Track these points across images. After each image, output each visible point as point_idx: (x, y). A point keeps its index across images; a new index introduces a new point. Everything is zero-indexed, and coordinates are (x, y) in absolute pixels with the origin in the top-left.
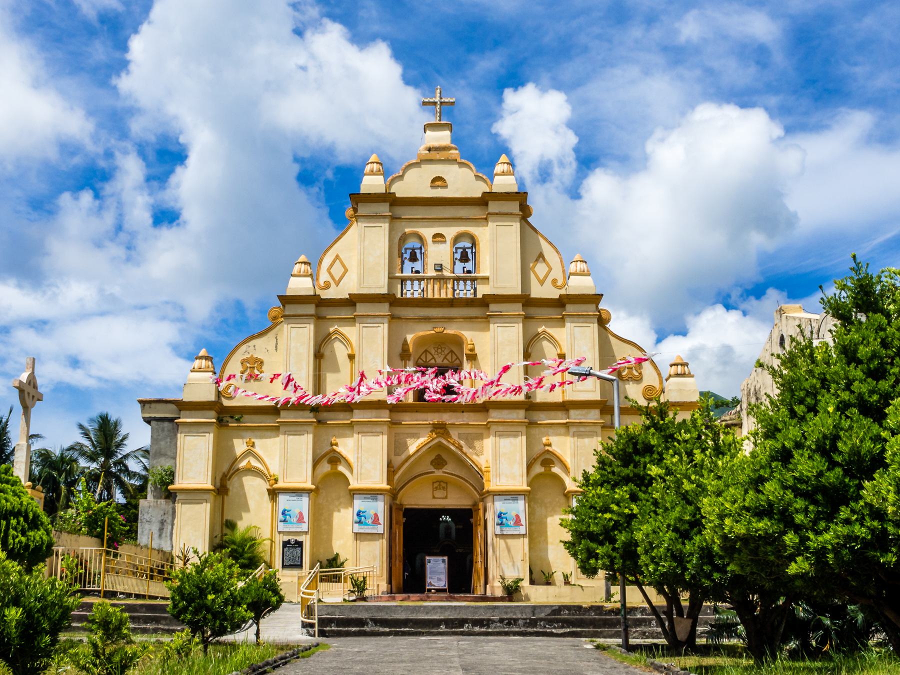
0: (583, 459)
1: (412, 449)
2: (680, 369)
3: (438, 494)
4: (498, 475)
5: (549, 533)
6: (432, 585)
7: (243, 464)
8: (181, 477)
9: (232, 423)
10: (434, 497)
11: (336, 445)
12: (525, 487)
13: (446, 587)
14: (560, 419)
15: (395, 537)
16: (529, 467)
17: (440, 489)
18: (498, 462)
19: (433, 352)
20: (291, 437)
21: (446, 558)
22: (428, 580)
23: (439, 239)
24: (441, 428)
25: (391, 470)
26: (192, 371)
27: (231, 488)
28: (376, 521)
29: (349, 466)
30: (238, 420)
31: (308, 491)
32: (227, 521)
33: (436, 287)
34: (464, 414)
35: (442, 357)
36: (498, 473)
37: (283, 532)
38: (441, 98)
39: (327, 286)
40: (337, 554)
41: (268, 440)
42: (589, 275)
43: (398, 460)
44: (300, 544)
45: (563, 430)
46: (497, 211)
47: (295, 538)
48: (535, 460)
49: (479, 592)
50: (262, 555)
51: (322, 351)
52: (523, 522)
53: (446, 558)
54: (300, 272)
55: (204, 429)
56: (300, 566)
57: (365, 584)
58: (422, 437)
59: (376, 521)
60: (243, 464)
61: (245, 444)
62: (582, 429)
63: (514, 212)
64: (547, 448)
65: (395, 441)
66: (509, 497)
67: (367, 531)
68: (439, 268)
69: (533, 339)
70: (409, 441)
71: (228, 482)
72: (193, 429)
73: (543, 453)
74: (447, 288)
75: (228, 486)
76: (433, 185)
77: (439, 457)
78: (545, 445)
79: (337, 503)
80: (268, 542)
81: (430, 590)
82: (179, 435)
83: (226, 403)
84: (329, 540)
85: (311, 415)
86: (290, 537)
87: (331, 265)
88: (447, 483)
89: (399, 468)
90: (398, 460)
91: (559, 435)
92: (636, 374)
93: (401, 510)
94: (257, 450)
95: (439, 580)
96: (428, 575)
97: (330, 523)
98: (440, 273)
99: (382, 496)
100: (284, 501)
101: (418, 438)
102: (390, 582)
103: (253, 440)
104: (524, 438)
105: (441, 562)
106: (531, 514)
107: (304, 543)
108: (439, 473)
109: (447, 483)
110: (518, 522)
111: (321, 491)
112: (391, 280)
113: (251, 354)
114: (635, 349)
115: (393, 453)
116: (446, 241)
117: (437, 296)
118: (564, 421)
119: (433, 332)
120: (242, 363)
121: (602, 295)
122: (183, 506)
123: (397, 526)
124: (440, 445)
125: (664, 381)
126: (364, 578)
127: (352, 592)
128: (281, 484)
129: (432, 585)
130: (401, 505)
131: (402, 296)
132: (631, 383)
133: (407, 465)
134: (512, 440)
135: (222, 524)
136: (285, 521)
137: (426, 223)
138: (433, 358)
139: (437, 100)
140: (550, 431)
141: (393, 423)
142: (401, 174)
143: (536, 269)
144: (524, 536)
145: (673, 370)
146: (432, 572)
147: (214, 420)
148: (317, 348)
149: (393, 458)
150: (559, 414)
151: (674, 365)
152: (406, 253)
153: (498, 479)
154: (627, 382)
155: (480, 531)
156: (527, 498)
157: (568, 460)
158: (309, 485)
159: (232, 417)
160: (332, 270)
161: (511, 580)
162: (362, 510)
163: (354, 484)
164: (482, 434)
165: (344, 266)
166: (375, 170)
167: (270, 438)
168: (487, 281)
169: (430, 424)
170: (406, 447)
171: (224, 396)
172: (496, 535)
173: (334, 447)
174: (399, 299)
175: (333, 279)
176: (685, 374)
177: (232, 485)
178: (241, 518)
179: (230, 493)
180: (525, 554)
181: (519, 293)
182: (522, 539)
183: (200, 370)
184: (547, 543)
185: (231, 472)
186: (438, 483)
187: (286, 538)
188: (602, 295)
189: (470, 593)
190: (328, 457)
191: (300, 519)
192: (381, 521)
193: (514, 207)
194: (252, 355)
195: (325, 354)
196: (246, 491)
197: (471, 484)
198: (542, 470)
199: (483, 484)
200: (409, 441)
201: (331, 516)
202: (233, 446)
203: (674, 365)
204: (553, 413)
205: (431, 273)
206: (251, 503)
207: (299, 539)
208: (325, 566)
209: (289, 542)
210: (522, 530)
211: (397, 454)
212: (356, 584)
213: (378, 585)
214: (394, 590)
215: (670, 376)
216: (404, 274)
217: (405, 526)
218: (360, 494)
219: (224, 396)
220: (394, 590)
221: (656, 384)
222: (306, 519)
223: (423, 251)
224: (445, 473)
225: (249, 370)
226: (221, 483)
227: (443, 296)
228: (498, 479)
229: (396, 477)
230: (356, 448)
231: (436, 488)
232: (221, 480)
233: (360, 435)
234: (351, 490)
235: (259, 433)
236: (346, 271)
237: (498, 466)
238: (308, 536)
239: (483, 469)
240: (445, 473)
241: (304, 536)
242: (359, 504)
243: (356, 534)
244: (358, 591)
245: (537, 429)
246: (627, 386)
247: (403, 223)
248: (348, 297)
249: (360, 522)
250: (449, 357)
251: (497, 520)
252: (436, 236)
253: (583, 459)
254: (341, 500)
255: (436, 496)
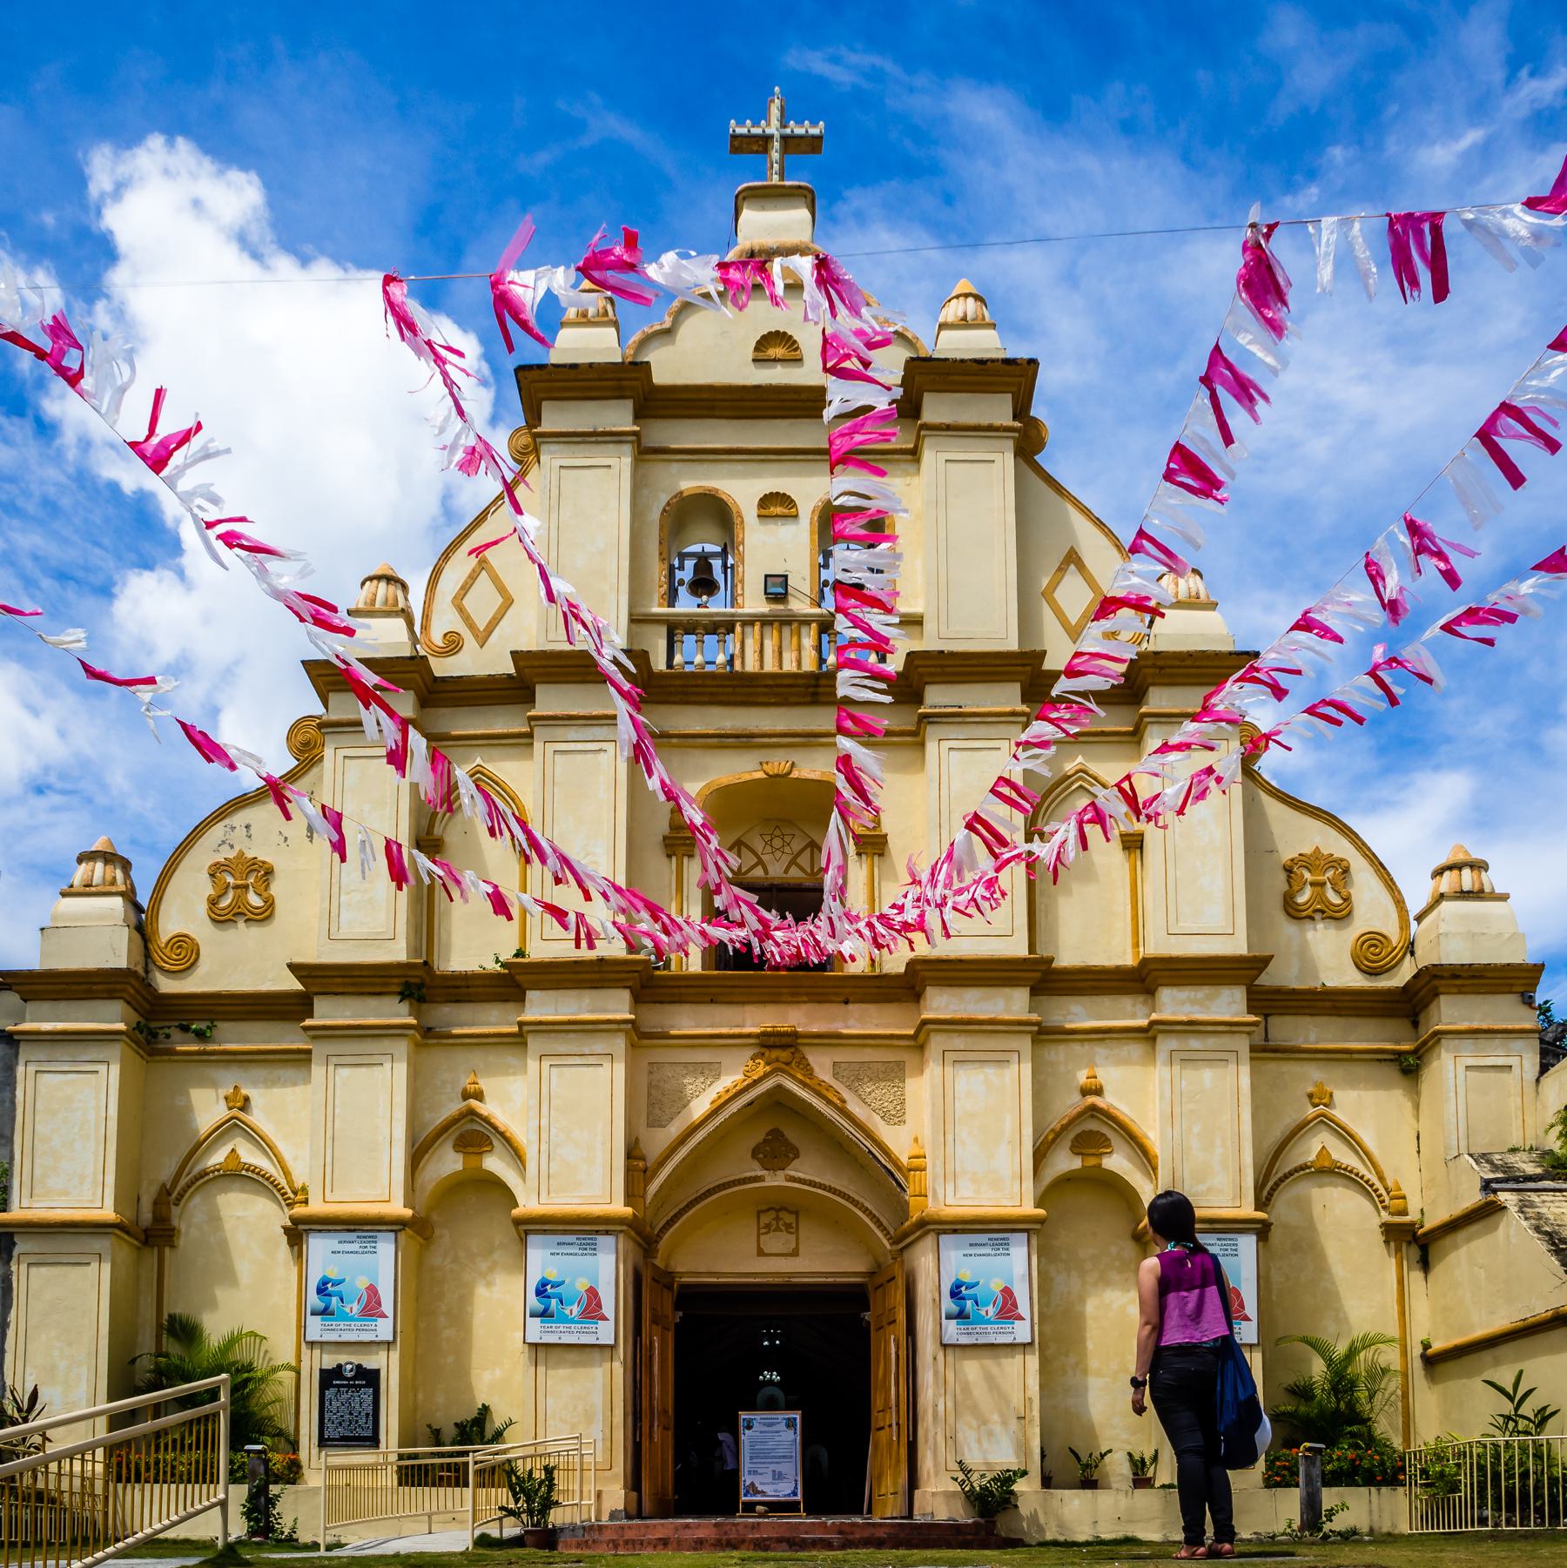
0: (1196, 1130)
1: (700, 1107)
2: (1467, 879)
3: (774, 1242)
4: (949, 1176)
5: (1090, 1345)
6: (757, 1492)
7: (218, 1158)
8: (26, 1191)
9: (183, 1043)
10: (761, 1253)
11: (479, 1096)
12: (1028, 1208)
13: (799, 1497)
14: (1129, 1013)
15: (651, 1357)
16: (1041, 1154)
17: (778, 1229)
18: (950, 1137)
19: (759, 845)
20: (344, 1072)
21: (797, 1415)
22: (746, 1479)
23: (779, 510)
24: (783, 1047)
25: (637, 1165)
26: (64, 895)
27: (183, 1228)
28: (592, 1309)
29: (517, 1155)
30: (201, 1036)
31: (393, 1225)
32: (172, 1318)
33: (769, 646)
34: (850, 1007)
35: (786, 859)
36: (950, 1167)
37: (322, 1344)
38: (784, 126)
39: (453, 645)
40: (485, 1410)
41: (289, 1090)
42: (1212, 606)
43: (658, 1140)
44: (370, 1378)
45: (1135, 1049)
46: (947, 420)
47: (357, 1360)
48: (1058, 1134)
49: (887, 1509)
50: (272, 1410)
51: (437, 831)
52: (1023, 1308)
53: (797, 1415)
54: (373, 602)
55: (93, 1052)
56: (373, 1441)
57: (551, 1487)
58: (728, 1074)
59: (592, 1309)
60: (218, 1158)
61: (223, 1103)
62: (1195, 1043)
63: (997, 422)
64: (1092, 1099)
65: (650, 1086)
66: (983, 1238)
67: (567, 1339)
68: (777, 587)
69: (1050, 791)
70: (690, 1084)
71: (175, 1211)
72: (62, 1052)
73: (1080, 1115)
74: (799, 649)
75: (175, 1222)
76: (761, 355)
77: (776, 1135)
78: (1085, 1092)
79: (483, 1266)
80: (287, 1377)
81: (750, 1507)
82: (20, 1069)
83: (167, 985)
84: (462, 1372)
85: (404, 1007)
86: (342, 1359)
87: (465, 589)
88: (797, 1213)
89: (661, 1163)
90: (658, 1140)
91: (1126, 1062)
92: (1336, 900)
93: (670, 1287)
94: (257, 1118)
95: (778, 1476)
96: (746, 1464)
97: (461, 1318)
98: (781, 607)
99: (610, 1240)
100: (319, 1247)
101: (718, 1076)
102: (634, 1482)
103: (244, 1091)
104: (1027, 1068)
105: (782, 1426)
106: (1045, 1286)
107: (383, 1375)
108: (775, 1180)
109: (797, 1213)
110: (1008, 1309)
111: (437, 1232)
112: (634, 626)
113: (237, 849)
114: (1333, 833)
115: (643, 1120)
116: (796, 516)
117: (770, 666)
118: (1144, 1022)
119: (760, 775)
120: (212, 875)
121: (303, 662)
122: (33, 1270)
123: (657, 1329)
124: (778, 1102)
125: (1414, 924)
126: (549, 1471)
127: (511, 1513)
128: (316, 1207)
129: (757, 1492)
130: (671, 1275)
131: (670, 664)
132: (1320, 926)
133: (683, 1152)
134: (990, 1072)
135: (159, 1326)
136: (325, 1312)
137: (740, 467)
138: (760, 862)
139: (773, 129)
140: (1100, 1051)
141: (639, 1036)
142: (667, 325)
143: (1058, 595)
144: (1025, 1347)
145: (1447, 883)
146: (757, 1455)
147: (121, 1026)
148: (425, 823)
149: (643, 1132)
150: (1127, 1002)
151: (1450, 868)
152: (681, 568)
153: (950, 1188)
154: (1308, 924)
155: (890, 1347)
156: (1034, 1241)
157: (1154, 1137)
158: (397, 1208)
159: (185, 1029)
160: (467, 603)
161: (989, 1476)
162: (553, 1277)
163: (529, 1203)
164: (900, 1065)
165: (501, 589)
166: (591, 311)
167: (295, 1084)
168: (917, 628)
169: (749, 1036)
170: (683, 1103)
171: (161, 969)
172: (945, 1346)
173: (473, 1103)
174: (661, 675)
175: (471, 626)
176: (1482, 891)
177: (190, 1219)
178: (212, 1304)
179: (182, 1242)
180: (1028, 1401)
181: (1013, 646)
182: (1019, 1358)
183: (88, 890)
184: (1085, 1372)
185: (183, 1181)
186: (772, 1214)
187: (330, 1361)
188: (303, 662)
189: (859, 1512)
190: (454, 1132)
191: (371, 1308)
192: (608, 1308)
193: (998, 410)
194: (241, 854)
195: (447, 839)
196: (229, 1235)
197: (866, 1210)
198: (1076, 1163)
199: (907, 1203)
200: (690, 1084)
201: (465, 1300)
202: (189, 1108)
203: (1450, 868)
204: (1106, 1002)
205: (754, 603)
206: (244, 1268)
207: (370, 1362)
208: (448, 1439)
209: (338, 1371)
210: (1021, 1331)
211: (655, 1122)
212: (523, 1490)
213: (599, 1495)
214: (647, 1506)
215: (1442, 897)
216: (677, 609)
217: (680, 1331)
218: (545, 1232)
219: (161, 969)
220: (647, 1506)
221: (1392, 931)
222: (387, 1306)
223: (730, 561)
224: (793, 1179)
225: (231, 894)
226: (154, 1213)
227: (789, 666)
228: (950, 1188)
229: (654, 1187)
230: (535, 1102)
231: (768, 1226)
232: (155, 1203)
233: (546, 1063)
234: (518, 1222)
235: (259, 1072)
236: (508, 602)
237: (950, 1149)
238: (395, 1356)
239: (904, 1160)
240: (793, 1179)
241: (383, 1355)
242: (542, 1259)
243: (535, 1346)
244: (530, 1512)
245: (1062, 1048)
246: (1310, 935)
247: (675, 467)
248: (510, 669)
249: (545, 1314)
250: (804, 860)
251: (948, 1304)
252: (768, 500)
253: (1196, 1130)
254: (496, 1256)
255: (766, 1251)
